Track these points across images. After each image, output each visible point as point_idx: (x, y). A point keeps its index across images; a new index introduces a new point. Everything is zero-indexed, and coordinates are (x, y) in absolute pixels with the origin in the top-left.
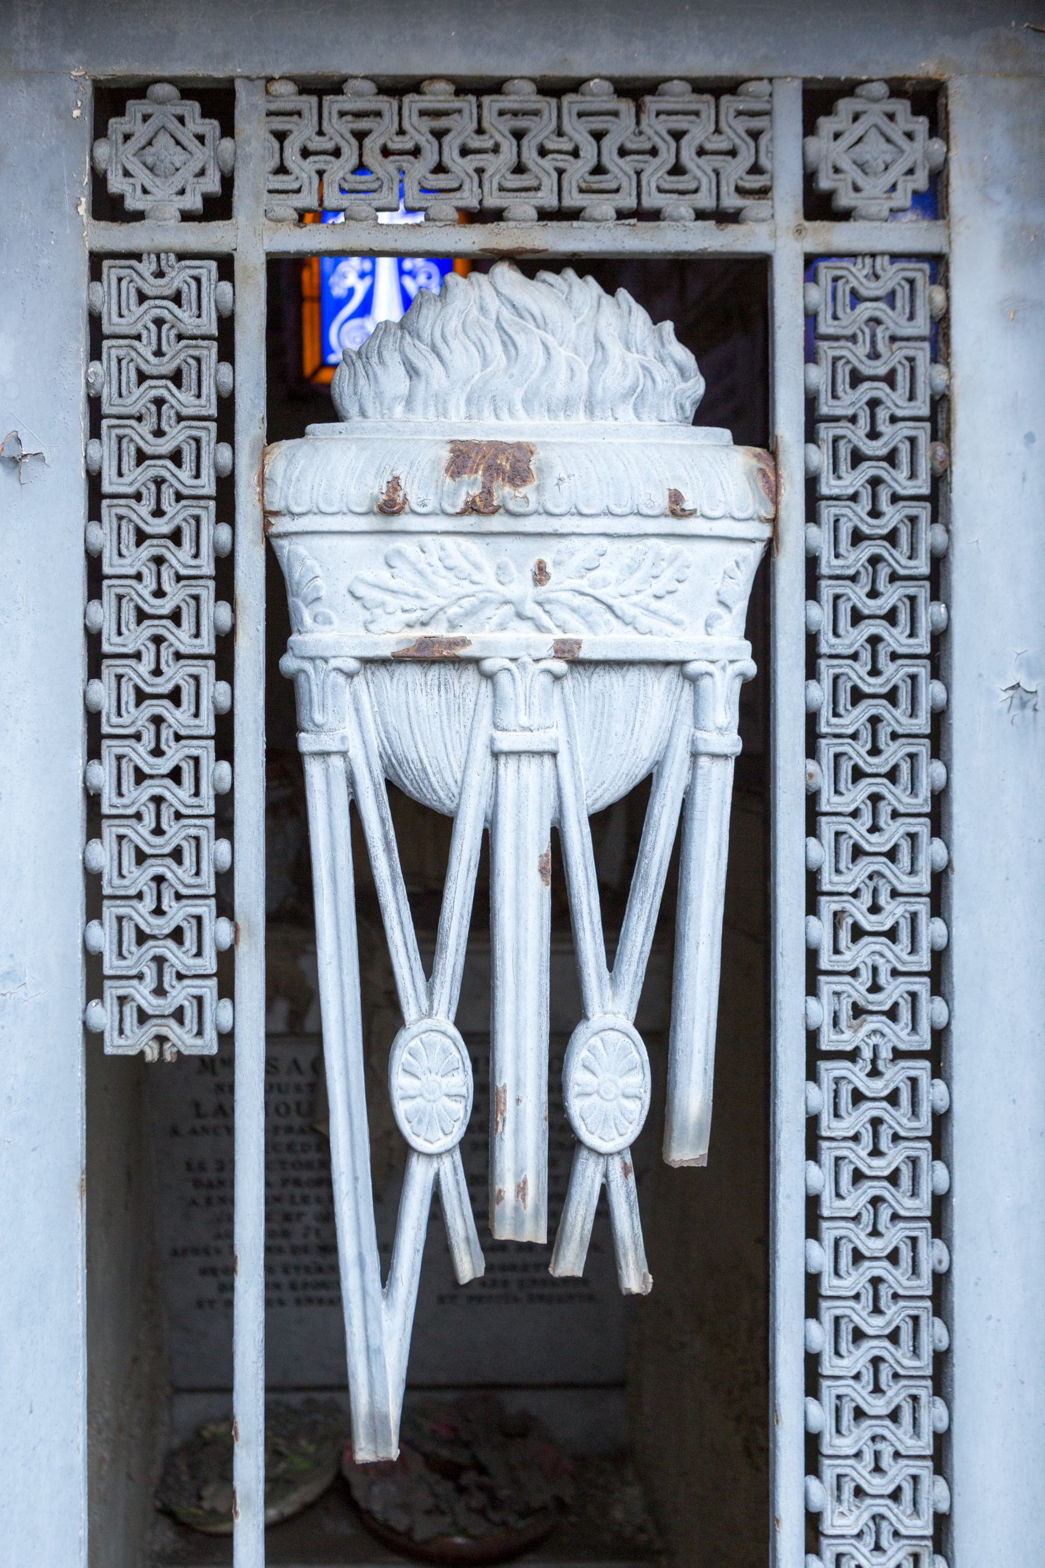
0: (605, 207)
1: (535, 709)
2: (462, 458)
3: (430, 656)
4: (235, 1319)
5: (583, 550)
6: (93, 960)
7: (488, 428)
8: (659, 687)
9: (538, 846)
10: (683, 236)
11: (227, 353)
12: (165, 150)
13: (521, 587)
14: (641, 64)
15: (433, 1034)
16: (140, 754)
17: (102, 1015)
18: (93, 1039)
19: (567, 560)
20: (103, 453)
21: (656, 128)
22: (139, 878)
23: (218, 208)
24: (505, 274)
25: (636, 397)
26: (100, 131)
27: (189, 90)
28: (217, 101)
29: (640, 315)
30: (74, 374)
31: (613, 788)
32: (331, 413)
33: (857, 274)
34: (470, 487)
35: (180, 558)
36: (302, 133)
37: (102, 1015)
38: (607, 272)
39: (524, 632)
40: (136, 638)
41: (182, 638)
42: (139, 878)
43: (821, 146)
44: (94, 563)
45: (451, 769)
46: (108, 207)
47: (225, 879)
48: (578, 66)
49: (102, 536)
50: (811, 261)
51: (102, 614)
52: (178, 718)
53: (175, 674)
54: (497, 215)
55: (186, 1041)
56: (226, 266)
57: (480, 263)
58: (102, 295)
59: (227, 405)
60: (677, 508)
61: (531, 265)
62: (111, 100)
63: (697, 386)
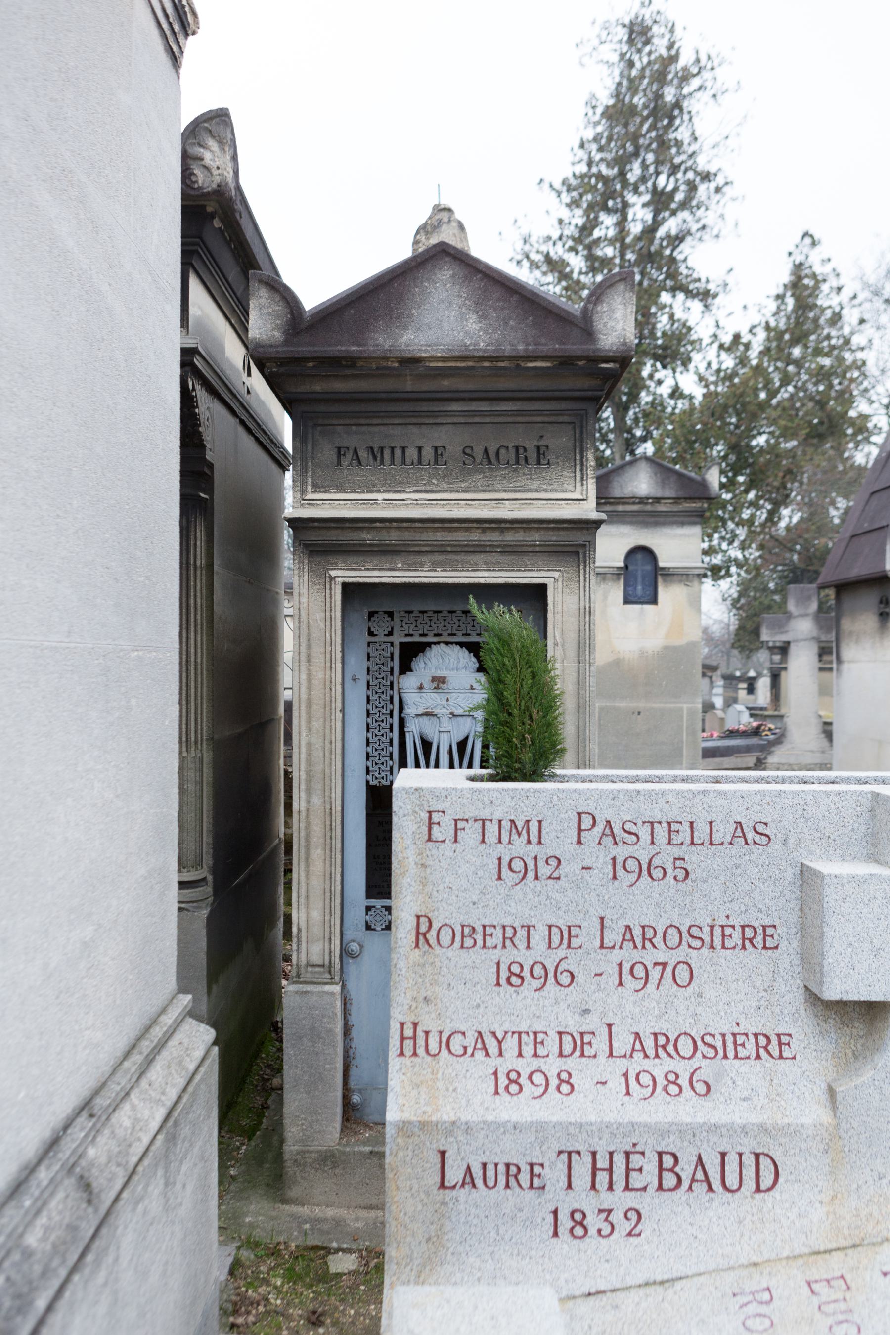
0: (460, 633)
1: (446, 725)
2: (434, 679)
3: (428, 714)
4: (395, 865)
5: (456, 695)
6: (368, 768)
7: (439, 674)
9: (447, 748)
10: (474, 639)
11: (392, 660)
12: (381, 623)
13: (444, 702)
15: (772, 1167)
16: (376, 731)
17: (369, 778)
18: (368, 782)
19: (453, 698)
20: (370, 678)
22: (376, 754)
23: (390, 634)
24: (442, 645)
25: (465, 667)
26: (369, 619)
28: (391, 614)
29: (467, 652)
30: (365, 664)
31: (461, 738)
32: (411, 671)
34: (435, 685)
35: (383, 697)
36: (406, 620)
37: (369, 778)
38: (461, 644)
39: (445, 710)
40: (376, 711)
41: (384, 711)
42: (376, 754)
44: (368, 697)
45: (431, 733)
46: (371, 634)
47: (391, 754)
48: (455, 608)
49: (370, 693)
51: (370, 707)
52: (383, 725)
53: (383, 717)
54: (440, 635)
55: (384, 782)
56: (392, 644)
57: (438, 643)
58: (370, 650)
59: (392, 669)
61: (447, 643)
62: (371, 615)
63: (477, 665)
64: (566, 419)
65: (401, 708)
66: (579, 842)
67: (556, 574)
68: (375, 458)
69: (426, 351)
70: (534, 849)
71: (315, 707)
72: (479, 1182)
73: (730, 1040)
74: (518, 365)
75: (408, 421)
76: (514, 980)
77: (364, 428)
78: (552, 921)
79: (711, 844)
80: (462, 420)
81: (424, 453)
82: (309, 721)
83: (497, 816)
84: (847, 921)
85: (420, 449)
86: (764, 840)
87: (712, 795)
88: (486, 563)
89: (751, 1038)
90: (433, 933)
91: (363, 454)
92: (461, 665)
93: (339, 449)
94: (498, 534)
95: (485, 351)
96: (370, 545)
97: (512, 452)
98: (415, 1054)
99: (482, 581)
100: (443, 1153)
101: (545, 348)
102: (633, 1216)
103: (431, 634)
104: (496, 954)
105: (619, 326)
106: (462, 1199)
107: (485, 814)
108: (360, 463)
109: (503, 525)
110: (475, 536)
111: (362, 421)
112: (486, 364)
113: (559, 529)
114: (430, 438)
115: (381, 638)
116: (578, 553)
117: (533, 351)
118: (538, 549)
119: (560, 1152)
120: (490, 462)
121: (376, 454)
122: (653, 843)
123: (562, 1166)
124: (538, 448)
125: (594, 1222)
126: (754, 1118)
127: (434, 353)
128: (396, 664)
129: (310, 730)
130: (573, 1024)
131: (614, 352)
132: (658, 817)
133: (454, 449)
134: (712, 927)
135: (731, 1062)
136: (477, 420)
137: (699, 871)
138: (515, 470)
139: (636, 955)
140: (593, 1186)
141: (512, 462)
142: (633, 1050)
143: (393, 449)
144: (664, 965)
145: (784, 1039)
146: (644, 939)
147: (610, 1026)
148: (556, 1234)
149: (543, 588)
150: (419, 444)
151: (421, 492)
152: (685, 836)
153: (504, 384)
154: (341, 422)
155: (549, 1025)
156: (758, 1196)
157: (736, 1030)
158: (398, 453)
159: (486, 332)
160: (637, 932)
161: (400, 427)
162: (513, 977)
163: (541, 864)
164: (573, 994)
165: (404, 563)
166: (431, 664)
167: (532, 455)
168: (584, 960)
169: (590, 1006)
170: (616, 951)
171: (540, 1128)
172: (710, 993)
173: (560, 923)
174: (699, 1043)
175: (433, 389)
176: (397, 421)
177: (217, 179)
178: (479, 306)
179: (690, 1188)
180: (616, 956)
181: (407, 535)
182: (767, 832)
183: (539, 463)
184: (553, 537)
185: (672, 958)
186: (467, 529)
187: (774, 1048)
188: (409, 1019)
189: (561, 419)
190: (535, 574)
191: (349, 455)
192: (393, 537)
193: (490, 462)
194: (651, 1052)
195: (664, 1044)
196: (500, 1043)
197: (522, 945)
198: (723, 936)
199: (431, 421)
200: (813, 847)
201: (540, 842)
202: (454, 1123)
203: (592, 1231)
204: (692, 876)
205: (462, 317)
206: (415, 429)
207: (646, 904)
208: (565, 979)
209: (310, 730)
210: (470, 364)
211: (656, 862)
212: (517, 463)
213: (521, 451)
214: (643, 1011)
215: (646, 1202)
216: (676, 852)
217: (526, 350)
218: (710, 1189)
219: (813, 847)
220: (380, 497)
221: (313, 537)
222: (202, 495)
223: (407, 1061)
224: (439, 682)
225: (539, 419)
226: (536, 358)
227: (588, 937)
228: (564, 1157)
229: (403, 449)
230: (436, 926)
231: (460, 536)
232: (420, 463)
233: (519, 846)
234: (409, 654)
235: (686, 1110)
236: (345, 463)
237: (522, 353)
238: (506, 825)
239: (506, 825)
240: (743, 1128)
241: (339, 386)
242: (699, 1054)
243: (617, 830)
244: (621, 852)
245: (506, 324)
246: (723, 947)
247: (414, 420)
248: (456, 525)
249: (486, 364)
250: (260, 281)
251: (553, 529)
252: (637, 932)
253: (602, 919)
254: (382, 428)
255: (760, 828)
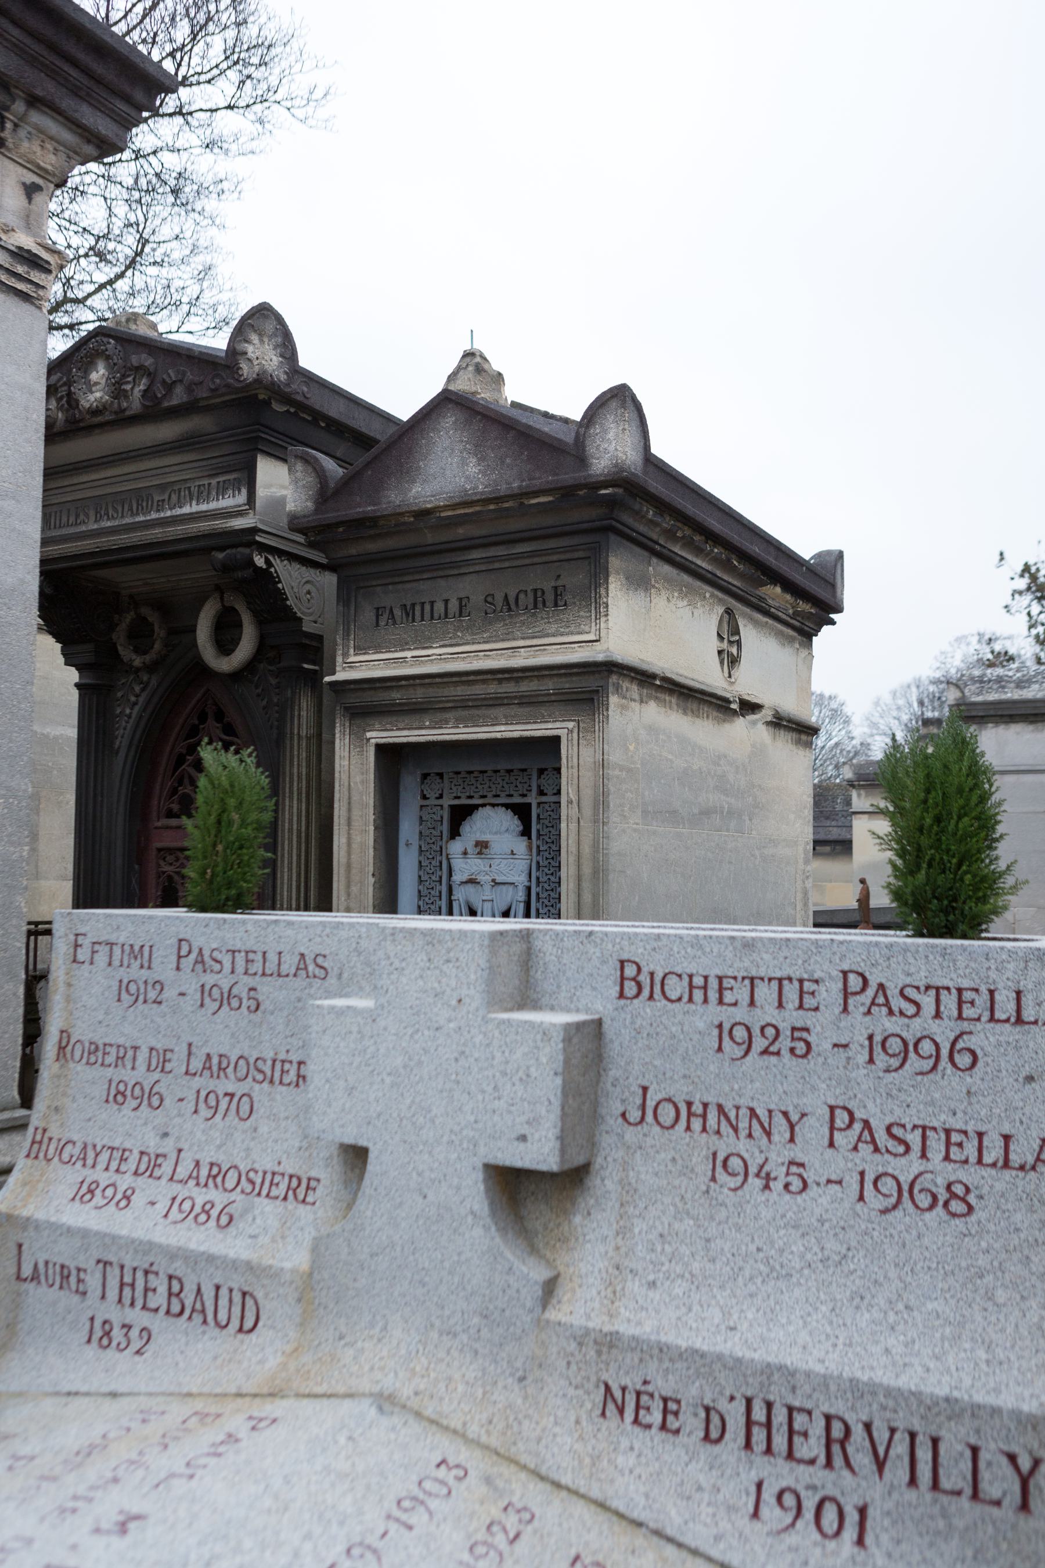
2: (478, 844)
5: (497, 861)
8: (511, 888)
10: (517, 800)
13: (487, 868)
14: (509, 767)
21: (512, 779)
23: (441, 797)
27: (438, 774)
28: (441, 775)
33: (547, 806)
38: (507, 806)
43: (542, 781)
50: (539, 804)
57: (484, 805)
60: (512, 853)
61: (493, 805)
62: (425, 776)
63: (521, 828)
64: (581, 554)
65: (450, 875)
66: (178, 969)
67: (571, 725)
68: (408, 615)
69: (430, 502)
70: (145, 973)
71: (354, 871)
72: (43, 1278)
73: (269, 1177)
74: (522, 504)
75: (435, 574)
76: (120, 1098)
77: (400, 586)
78: (153, 1044)
79: (279, 975)
80: (483, 567)
81: (450, 606)
82: (348, 886)
83: (121, 940)
84: (326, 1054)
85: (446, 601)
86: (322, 973)
87: (283, 924)
88: (506, 717)
89: (287, 1178)
90: (69, 1048)
91: (398, 612)
92: (503, 829)
93: (378, 609)
94: (513, 684)
95: (482, 493)
96: (400, 704)
97: (531, 595)
98: (36, 1157)
99: (499, 735)
100: (20, 1246)
101: (537, 482)
102: (145, 1334)
103: (476, 795)
104: (109, 1072)
105: (612, 448)
106: (31, 1292)
107: (113, 938)
108: (395, 623)
109: (515, 675)
110: (492, 688)
111: (397, 579)
112: (492, 507)
113: (571, 674)
114: (453, 590)
115: (433, 801)
116: (592, 699)
117: (527, 486)
118: (553, 698)
119: (99, 1261)
120: (510, 609)
121: (408, 612)
122: (233, 972)
123: (98, 1275)
124: (556, 588)
125: (117, 1334)
126: (245, 1255)
127: (437, 503)
128: (445, 827)
129: (349, 895)
130: (153, 1144)
131: (608, 474)
132: (239, 945)
133: (477, 599)
134: (274, 1061)
135: (263, 1201)
136: (497, 565)
137: (268, 1002)
138: (534, 615)
139: (212, 1084)
140: (120, 1301)
141: (531, 606)
142: (190, 1177)
143: (423, 604)
144: (232, 1095)
145: (313, 1184)
146: (220, 1069)
147: (180, 1151)
148: (89, 1341)
149: (555, 741)
150: (445, 596)
151: (451, 646)
152: (257, 967)
153: (515, 525)
154: (379, 582)
155: (135, 1145)
156: (240, 1336)
157: (277, 1169)
158: (427, 607)
159: (484, 474)
160: (215, 1061)
161: (429, 582)
162: (118, 1096)
163: (149, 987)
164: (159, 1118)
165: (431, 721)
166: (476, 828)
167: (550, 597)
168: (175, 1087)
169: (169, 1130)
170: (197, 1078)
171: (84, 1234)
172: (263, 1129)
173: (159, 1046)
174: (243, 1178)
175: (444, 539)
176: (425, 576)
177: (257, 369)
178: (479, 449)
179: (190, 1318)
180: (197, 1082)
181: (432, 692)
182: (325, 965)
183: (556, 605)
184: (566, 684)
185: (239, 1089)
186: (484, 681)
187: (301, 1192)
188: (42, 1125)
189: (576, 555)
190: (550, 726)
191: (386, 616)
192: (418, 695)
193: (510, 609)
194: (203, 1181)
195: (216, 1175)
196: (97, 1155)
197: (129, 1066)
198: (282, 1071)
199: (456, 572)
200: (364, 983)
201: (149, 968)
202: (28, 1219)
203: (114, 1344)
204: (262, 1008)
205: (464, 463)
206: (442, 583)
207: (223, 1033)
208: (155, 1101)
209: (349, 895)
210: (478, 508)
211: (235, 991)
212: (535, 607)
213: (539, 594)
214: (206, 1140)
215: (157, 1323)
216: (251, 981)
217: (520, 487)
218: (205, 1322)
219: (364, 983)
220: (408, 654)
221: (353, 699)
222: (306, 666)
223: (29, 1162)
224: (482, 846)
225: (555, 558)
226: (536, 493)
227: (177, 1064)
228: (101, 1265)
229: (432, 603)
230: (72, 1042)
231: (478, 690)
232: (446, 616)
233: (135, 971)
234: (460, 815)
235: (201, 1239)
236: (382, 623)
237: (516, 491)
238: (127, 948)
239: (127, 948)
240: (234, 1262)
241: (371, 547)
242: (239, 1189)
243: (207, 958)
244: (210, 979)
245: (503, 462)
246: (281, 1083)
247: (441, 573)
248: (472, 678)
249: (492, 507)
250: (296, 457)
251: (565, 675)
252: (215, 1061)
253: (190, 1045)
254: (414, 585)
255: (320, 960)
